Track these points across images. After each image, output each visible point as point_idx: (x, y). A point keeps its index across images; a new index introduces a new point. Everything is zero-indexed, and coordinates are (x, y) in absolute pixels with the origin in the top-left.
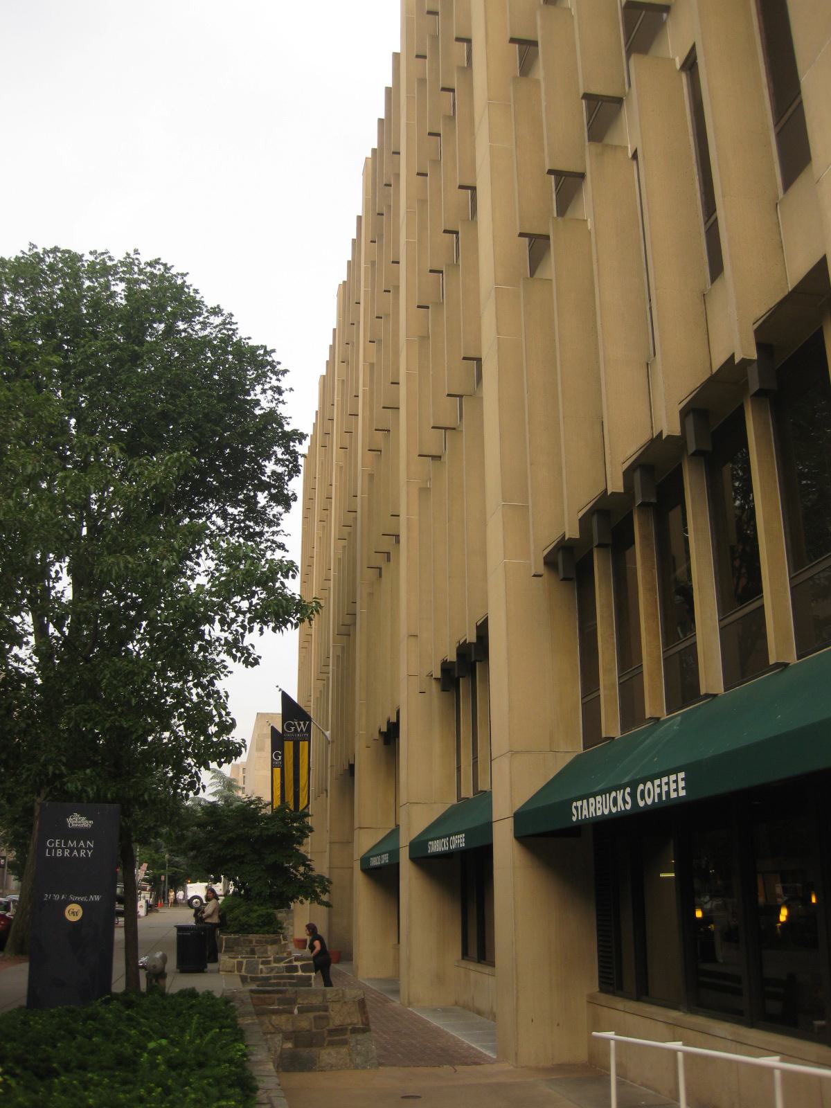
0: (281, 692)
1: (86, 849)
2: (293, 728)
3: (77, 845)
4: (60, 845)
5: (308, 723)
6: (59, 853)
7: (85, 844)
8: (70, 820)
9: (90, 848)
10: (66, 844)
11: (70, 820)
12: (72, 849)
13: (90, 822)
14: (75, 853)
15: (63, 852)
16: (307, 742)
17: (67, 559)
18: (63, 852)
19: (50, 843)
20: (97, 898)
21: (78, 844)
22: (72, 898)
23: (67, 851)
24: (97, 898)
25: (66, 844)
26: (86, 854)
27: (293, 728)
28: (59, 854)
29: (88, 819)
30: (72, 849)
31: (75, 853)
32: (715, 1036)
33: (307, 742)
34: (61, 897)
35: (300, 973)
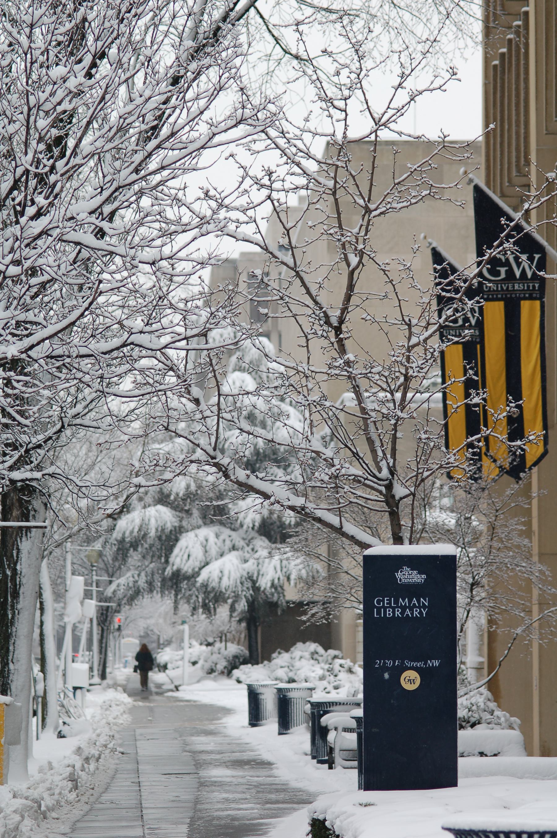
0: (471, 187)
1: (419, 607)
2: (503, 270)
3: (410, 603)
4: (390, 603)
5: (537, 256)
6: (389, 613)
7: (419, 601)
8: (399, 575)
9: (424, 606)
10: (396, 602)
11: (399, 575)
12: (404, 608)
13: (423, 576)
14: (408, 612)
15: (394, 612)
16: (538, 303)
17: (498, 268)
18: (394, 612)
19: (378, 602)
20: (436, 663)
21: (410, 602)
22: (407, 663)
23: (398, 611)
24: (436, 663)
25: (396, 602)
26: (421, 613)
27: (503, 270)
28: (389, 614)
29: (419, 573)
30: (404, 608)
31: (408, 612)
32: (193, 241)
33: (538, 303)
34: (394, 663)
35: (362, 730)
